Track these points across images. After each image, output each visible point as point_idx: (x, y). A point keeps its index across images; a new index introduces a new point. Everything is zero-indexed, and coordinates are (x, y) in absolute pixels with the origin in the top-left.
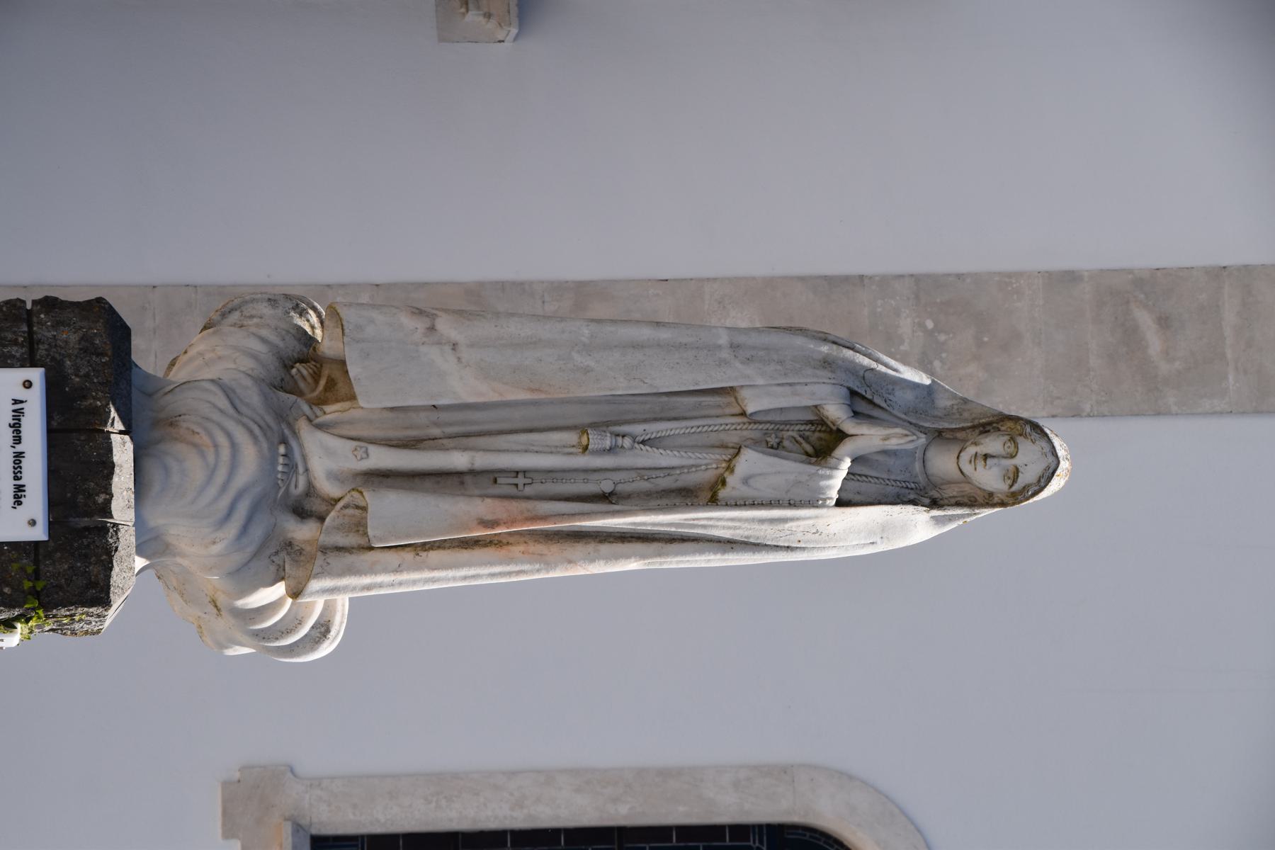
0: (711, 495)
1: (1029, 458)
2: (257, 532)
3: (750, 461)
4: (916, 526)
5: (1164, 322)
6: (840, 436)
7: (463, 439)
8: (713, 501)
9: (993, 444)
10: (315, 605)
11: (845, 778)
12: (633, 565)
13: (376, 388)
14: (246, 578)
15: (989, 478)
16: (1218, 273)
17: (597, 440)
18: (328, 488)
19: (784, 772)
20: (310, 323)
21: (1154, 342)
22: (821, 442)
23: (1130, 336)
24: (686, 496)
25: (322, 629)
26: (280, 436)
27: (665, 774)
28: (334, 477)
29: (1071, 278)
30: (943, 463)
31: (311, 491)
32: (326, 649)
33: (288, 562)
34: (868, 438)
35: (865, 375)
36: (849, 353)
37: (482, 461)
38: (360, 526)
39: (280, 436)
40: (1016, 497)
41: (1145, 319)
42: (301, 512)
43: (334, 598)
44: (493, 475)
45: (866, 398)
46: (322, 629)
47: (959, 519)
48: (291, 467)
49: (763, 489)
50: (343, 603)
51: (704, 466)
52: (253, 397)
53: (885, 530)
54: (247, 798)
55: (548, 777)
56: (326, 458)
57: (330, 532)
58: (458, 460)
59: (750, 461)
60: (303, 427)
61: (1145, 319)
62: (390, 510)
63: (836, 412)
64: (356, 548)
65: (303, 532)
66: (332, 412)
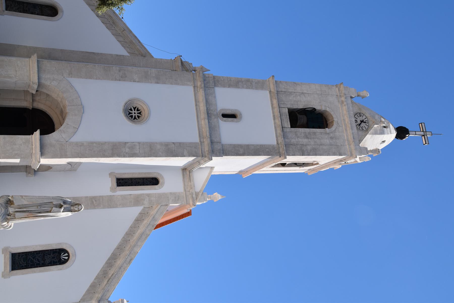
0: (50, 212)
1: (80, 207)
2: (4, 217)
3: (54, 208)
4: (70, 214)
5: (95, 201)
6: (63, 206)
7: (25, 208)
8: (50, 212)
9: (77, 206)
10: (10, 224)
11: (66, 244)
12: (42, 219)
13: (16, 203)
14: (3, 222)
15: (76, 209)
16: (100, 196)
17: (39, 207)
18: (11, 213)
19: (61, 244)
20: (10, 198)
21: (95, 202)
22: (61, 206)
23: (93, 202)
24: (48, 212)
25: (11, 226)
26: (6, 208)
27: (49, 245)
28: (12, 212)
29: (87, 197)
30: (72, 208)
31: (9, 213)
32: (11, 228)
33: (7, 220)
34: (65, 206)
35: (64, 200)
36: (105, 283)
37: (27, 209)
38: (15, 216)
39: (6, 208)
40: (79, 211)
41: (94, 200)
42: (8, 215)
43: (12, 223)
44: (28, 211)
45: (65, 202)
46: (11, 226)
47: (74, 213)
48: (7, 211)
49: (55, 211)
50: (13, 224)
51: (49, 209)
52: (4, 205)
53: (67, 214)
54: (4, 250)
55: (36, 246)
56: (11, 210)
57: (12, 217)
58: (25, 210)
59: (54, 208)
60: (9, 207)
61: (94, 200)
62: (17, 215)
63: (62, 204)
64: (14, 218)
65: (9, 217)
66: (12, 206)
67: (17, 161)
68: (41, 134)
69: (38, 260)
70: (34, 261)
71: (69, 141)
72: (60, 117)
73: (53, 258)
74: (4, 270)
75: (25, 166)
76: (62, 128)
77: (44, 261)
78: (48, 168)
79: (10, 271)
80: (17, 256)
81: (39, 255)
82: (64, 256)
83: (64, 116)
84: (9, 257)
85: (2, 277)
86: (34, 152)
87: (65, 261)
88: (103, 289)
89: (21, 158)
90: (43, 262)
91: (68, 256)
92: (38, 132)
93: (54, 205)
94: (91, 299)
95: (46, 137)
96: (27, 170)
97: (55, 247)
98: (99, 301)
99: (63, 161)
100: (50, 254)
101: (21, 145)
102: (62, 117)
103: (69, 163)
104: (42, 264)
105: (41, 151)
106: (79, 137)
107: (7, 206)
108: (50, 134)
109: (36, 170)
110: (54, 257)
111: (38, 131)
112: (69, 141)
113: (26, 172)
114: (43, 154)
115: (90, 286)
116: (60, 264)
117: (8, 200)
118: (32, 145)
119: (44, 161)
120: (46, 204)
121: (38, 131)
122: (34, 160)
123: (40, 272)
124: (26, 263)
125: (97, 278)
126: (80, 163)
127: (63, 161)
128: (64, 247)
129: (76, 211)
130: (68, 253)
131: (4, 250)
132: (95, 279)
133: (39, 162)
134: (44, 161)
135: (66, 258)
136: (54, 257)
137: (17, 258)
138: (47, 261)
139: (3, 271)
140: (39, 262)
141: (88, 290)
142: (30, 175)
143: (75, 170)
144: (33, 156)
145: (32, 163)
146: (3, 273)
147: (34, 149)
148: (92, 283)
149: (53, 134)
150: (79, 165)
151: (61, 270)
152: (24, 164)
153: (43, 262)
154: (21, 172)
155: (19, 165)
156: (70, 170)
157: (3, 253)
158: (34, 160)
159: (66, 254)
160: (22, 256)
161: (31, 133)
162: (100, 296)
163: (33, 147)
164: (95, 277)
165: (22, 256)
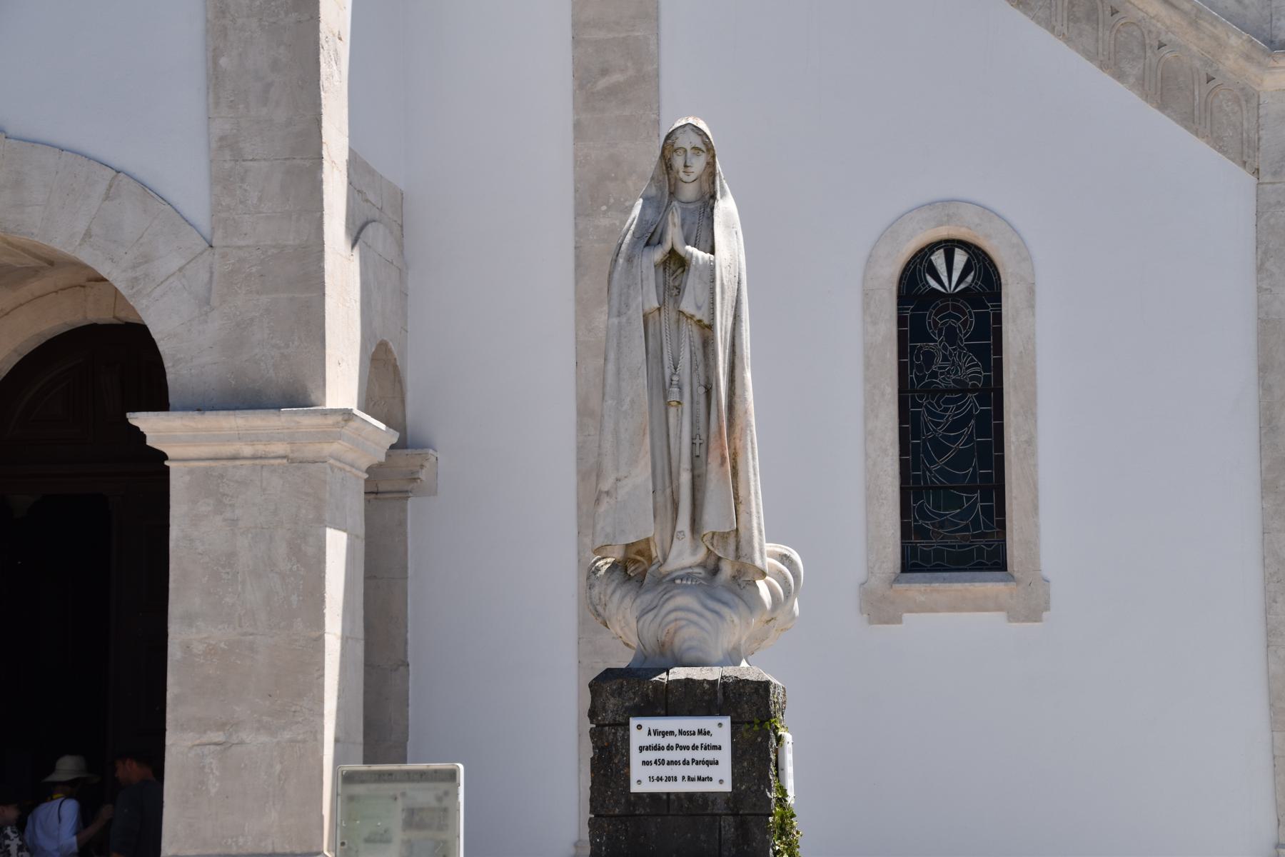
0: (707, 329)
2: (727, 596)
3: (687, 305)
4: (726, 207)
5: (604, 72)
6: (673, 252)
7: (672, 475)
9: (678, 162)
10: (770, 563)
11: (870, 261)
12: (748, 375)
13: (641, 525)
14: (753, 602)
15: (698, 164)
16: (576, 41)
17: (674, 397)
18: (701, 555)
19: (867, 295)
20: (604, 565)
21: (616, 78)
22: (676, 263)
23: (612, 91)
24: (707, 343)
25: (784, 559)
26: (670, 583)
28: (695, 550)
29: (577, 126)
30: (689, 191)
31: (702, 565)
32: (796, 557)
33: (745, 578)
34: (674, 235)
35: (633, 244)
38: (724, 536)
39: (670, 583)
40: (710, 149)
41: (603, 83)
42: (715, 571)
43: (766, 552)
44: (694, 458)
45: (650, 236)
46: (784, 559)
47: (722, 182)
48: (688, 576)
49: (704, 298)
50: (769, 547)
51: (690, 334)
52: (647, 598)
53: (728, 226)
54: (879, 610)
55: (869, 435)
56: (683, 556)
58: (685, 478)
59: (687, 305)
61: (603, 83)
62: (713, 520)
63: (658, 254)
64: (736, 538)
65: (727, 570)
66: (656, 552)
67: (337, 545)
68: (158, 400)
69: (958, 425)
70: (960, 445)
71: (206, 229)
72: (35, 286)
73: (951, 336)
74: (999, 608)
75: (367, 502)
76: (117, 276)
77: (964, 391)
78: (383, 371)
79: (1012, 578)
80: (921, 543)
81: (926, 417)
82: (950, 276)
83: (31, 262)
84: (921, 588)
85: (1038, 619)
86: (279, 448)
87: (984, 269)
88: (1194, 20)
89: (322, 523)
90: (971, 396)
91: (949, 246)
92: (149, 424)
93: (662, 304)
94: (1247, 97)
95: (176, 374)
96: (389, 494)
97: (887, 328)
98: (1275, 46)
99: (342, 271)
100: (929, 357)
101: (234, 522)
102: (35, 272)
103: (356, 234)
104: (983, 399)
105: (276, 406)
106: (182, 170)
107: (659, 581)
108: (162, 347)
109: (394, 437)
110: (950, 332)
111: (144, 421)
112: (206, 229)
113: (404, 494)
114: (296, 395)
115: (1162, 107)
116: (997, 297)
117: (618, 575)
118: (234, 458)
119: (342, 386)
120: (654, 356)
121: (144, 421)
122: (335, 447)
123: (1030, 410)
124: (971, 490)
125: (1112, 64)
126: (355, 164)
127: (342, 271)
128: (891, 271)
129: (711, 165)
130: (932, 247)
131: (879, 610)
132: (1120, 76)
133: (347, 414)
134: (342, 386)
135: (960, 258)
136: (950, 332)
137: (935, 543)
138: (969, 370)
139: (1000, 617)
140: (970, 415)
141: (1189, 120)
142: (423, 475)
143: (399, 199)
144: (310, 450)
145: (350, 456)
146: (1013, 617)
147: (261, 448)
148: (1146, 97)
149: (157, 332)
150: (371, 172)
151: (1031, 290)
152: (355, 503)
153: (971, 396)
154: (402, 523)
155: (361, 531)
156: (400, 232)
157: (898, 620)
158: (335, 447)
159: (938, 259)
160: (924, 516)
161: (154, 465)
162: (1236, 41)
163: (247, 450)
164: (1106, 79)
165: (924, 516)
